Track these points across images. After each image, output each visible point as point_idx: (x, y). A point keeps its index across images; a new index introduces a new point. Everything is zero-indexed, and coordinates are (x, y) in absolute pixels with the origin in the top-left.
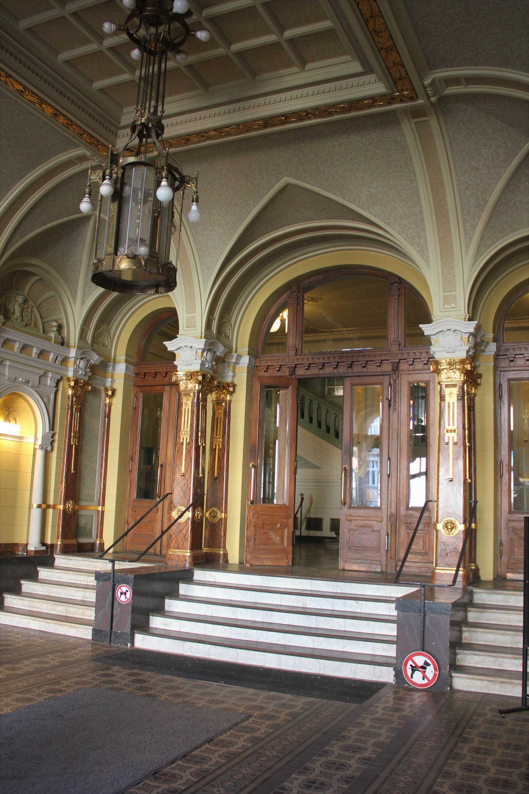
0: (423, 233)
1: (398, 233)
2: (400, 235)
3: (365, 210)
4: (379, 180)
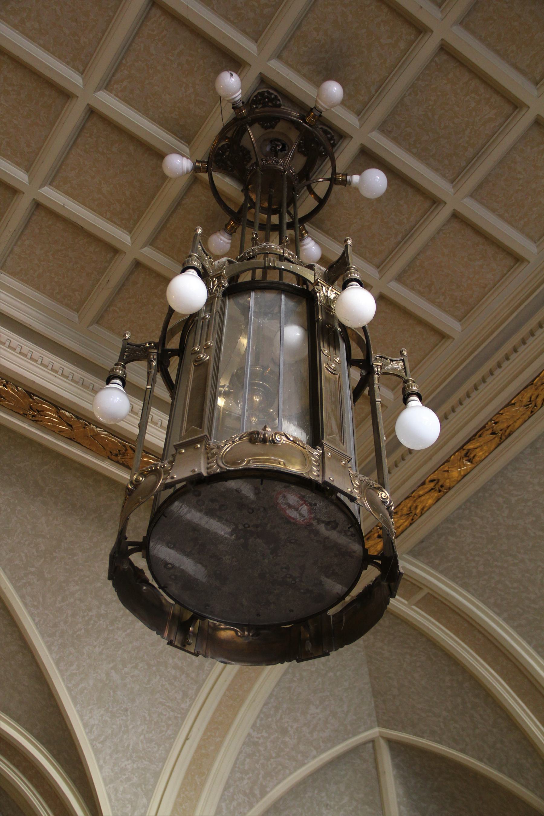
0: (145, 800)
1: (104, 780)
2: (106, 785)
3: (75, 704)
4: (141, 665)
